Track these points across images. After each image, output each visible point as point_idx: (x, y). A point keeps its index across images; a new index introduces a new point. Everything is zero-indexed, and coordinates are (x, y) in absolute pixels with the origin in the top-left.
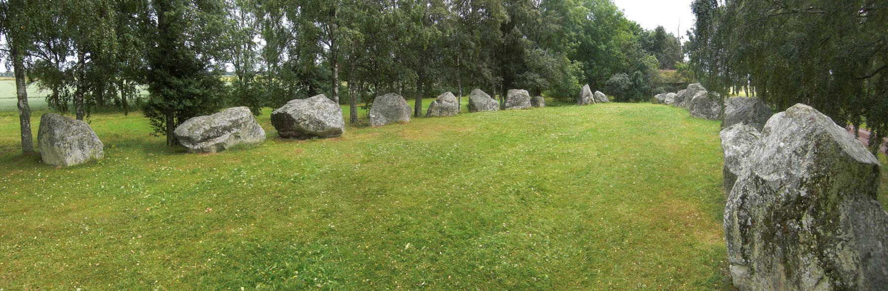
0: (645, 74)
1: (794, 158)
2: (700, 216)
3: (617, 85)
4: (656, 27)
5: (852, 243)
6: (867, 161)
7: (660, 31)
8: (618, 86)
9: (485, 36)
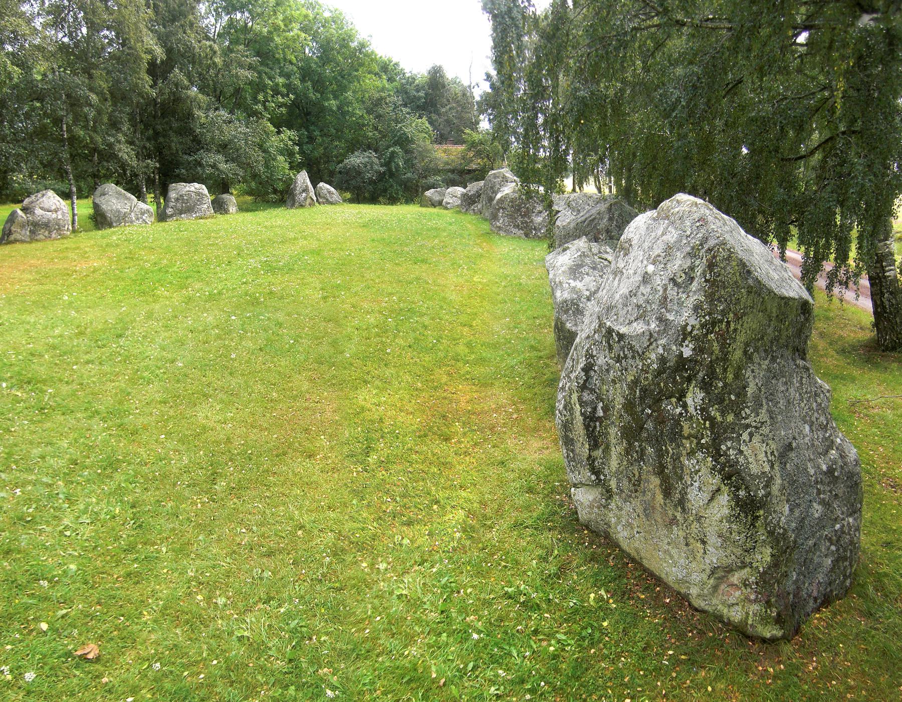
0: (407, 152)
1: (672, 292)
2: (518, 411)
3: (357, 172)
4: (429, 67)
5: (765, 430)
6: (792, 294)
8: (359, 173)
9: (117, 82)
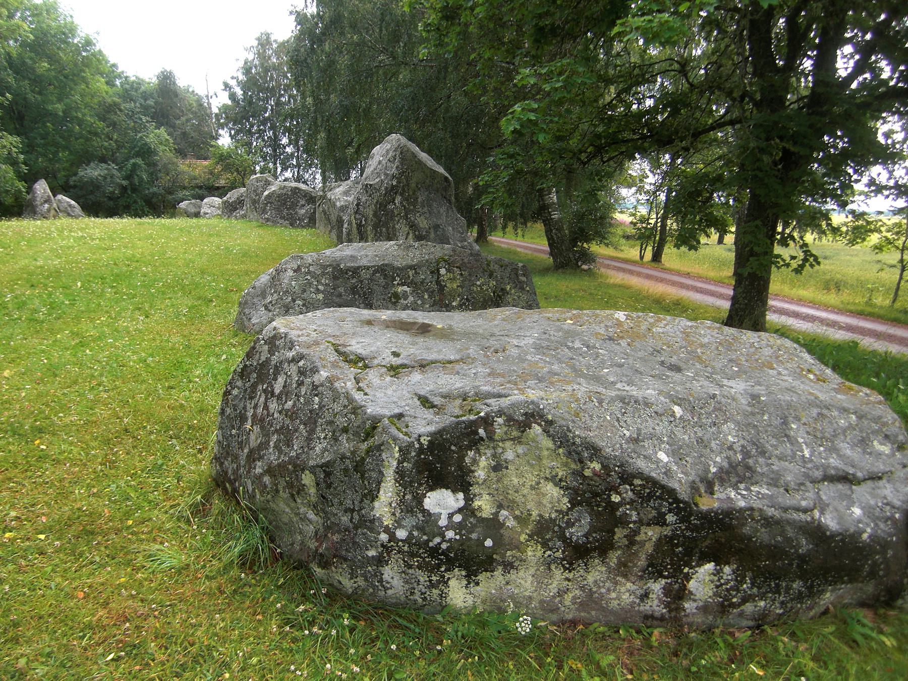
1: (389, 164)
4: (158, 71)
7: (166, 79)
